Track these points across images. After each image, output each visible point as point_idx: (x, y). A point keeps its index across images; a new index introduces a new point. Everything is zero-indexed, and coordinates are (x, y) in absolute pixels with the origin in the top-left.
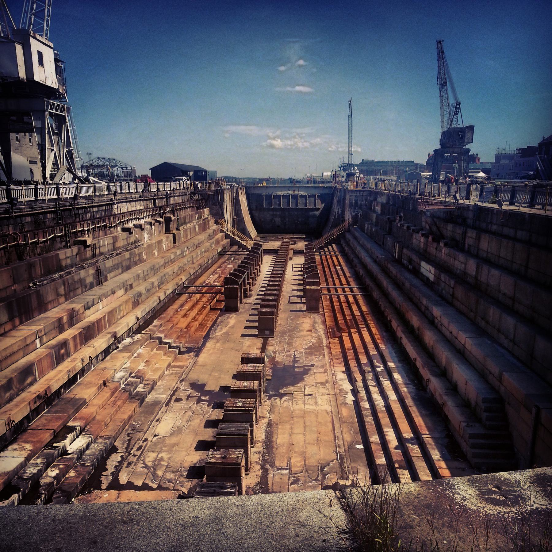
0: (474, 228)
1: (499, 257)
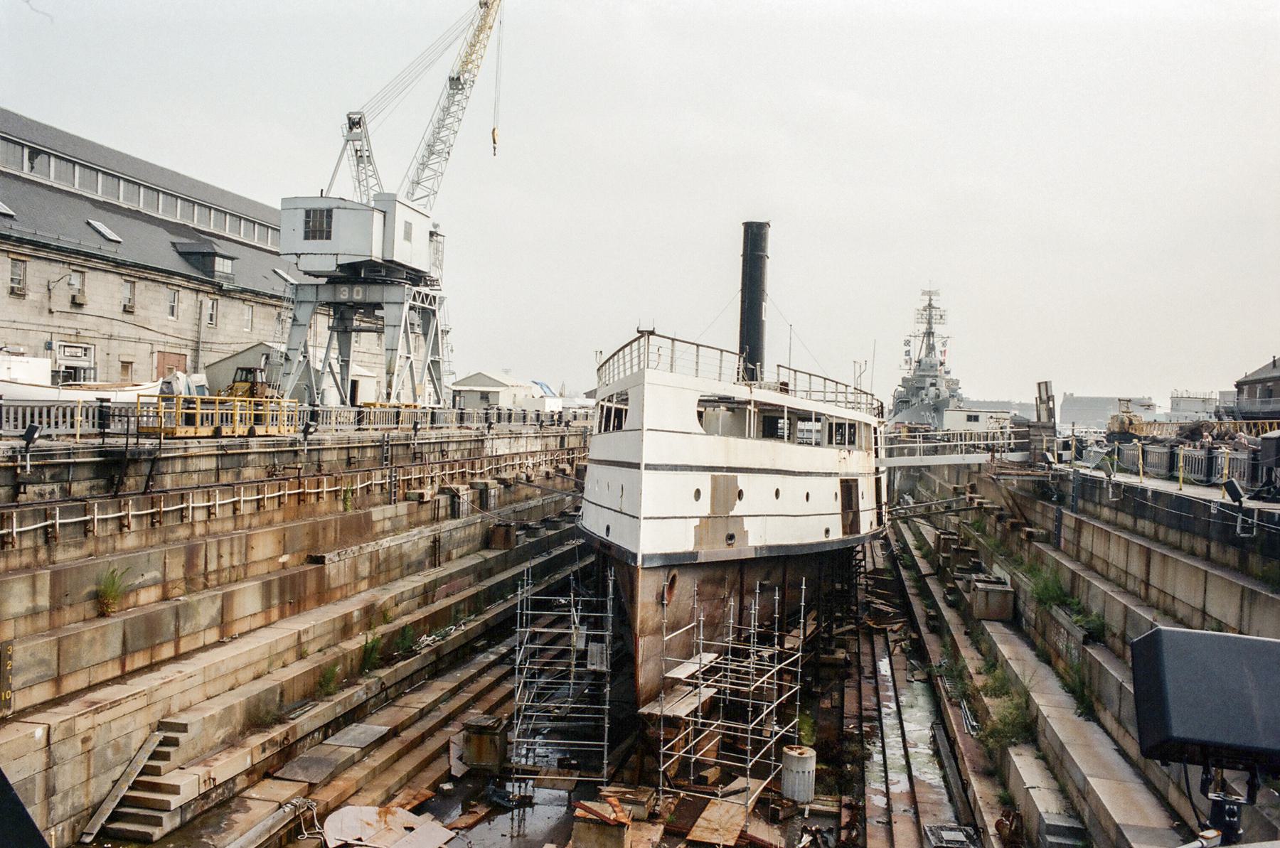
0: (1074, 509)
1: (1126, 572)
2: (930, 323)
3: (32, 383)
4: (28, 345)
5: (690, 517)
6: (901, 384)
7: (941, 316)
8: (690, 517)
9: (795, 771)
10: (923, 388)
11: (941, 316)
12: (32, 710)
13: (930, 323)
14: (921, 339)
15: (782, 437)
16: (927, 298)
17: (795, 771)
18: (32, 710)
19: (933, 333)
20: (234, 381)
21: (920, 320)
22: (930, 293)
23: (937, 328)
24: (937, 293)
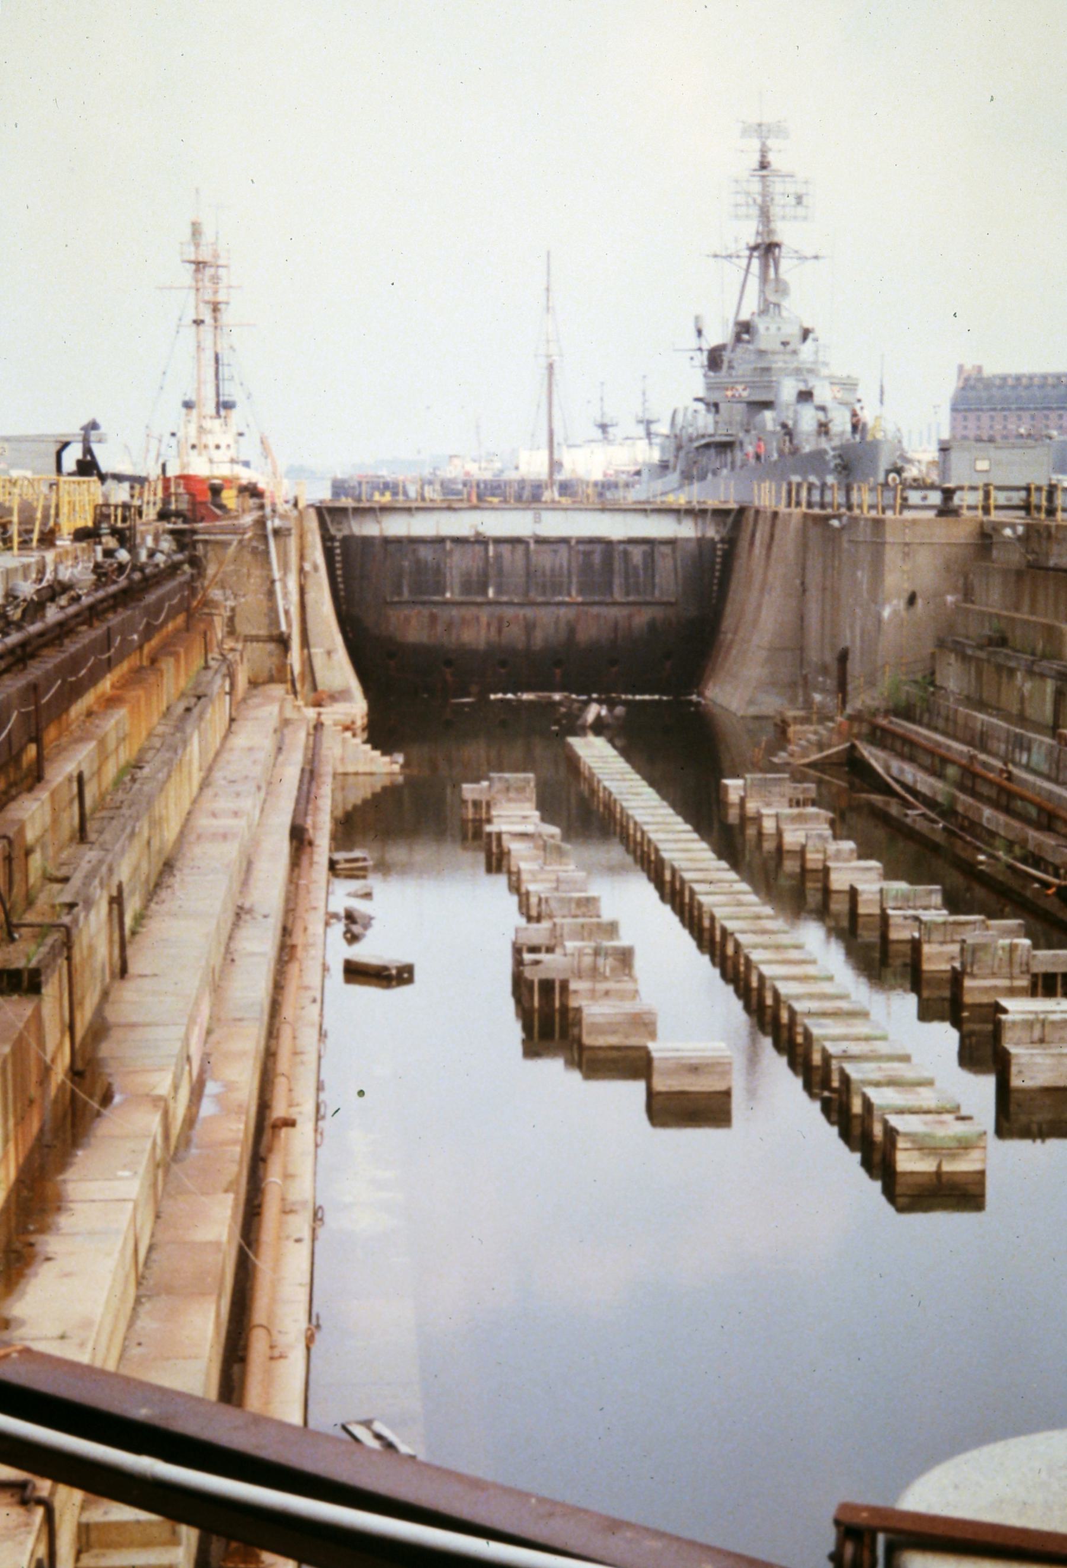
2: (765, 215)
3: (316, 1266)
4: (103, 478)
5: (548, 274)
6: (701, 394)
7: (799, 199)
8: (548, 274)
9: (212, 446)
10: (768, 405)
11: (799, 199)
12: (1033, 812)
13: (765, 215)
14: (744, 262)
15: (367, 483)
16: (756, 144)
17: (212, 446)
18: (1033, 812)
19: (777, 245)
20: (158, 750)
21: (743, 210)
22: (761, 130)
23: (785, 232)
24: (779, 131)
